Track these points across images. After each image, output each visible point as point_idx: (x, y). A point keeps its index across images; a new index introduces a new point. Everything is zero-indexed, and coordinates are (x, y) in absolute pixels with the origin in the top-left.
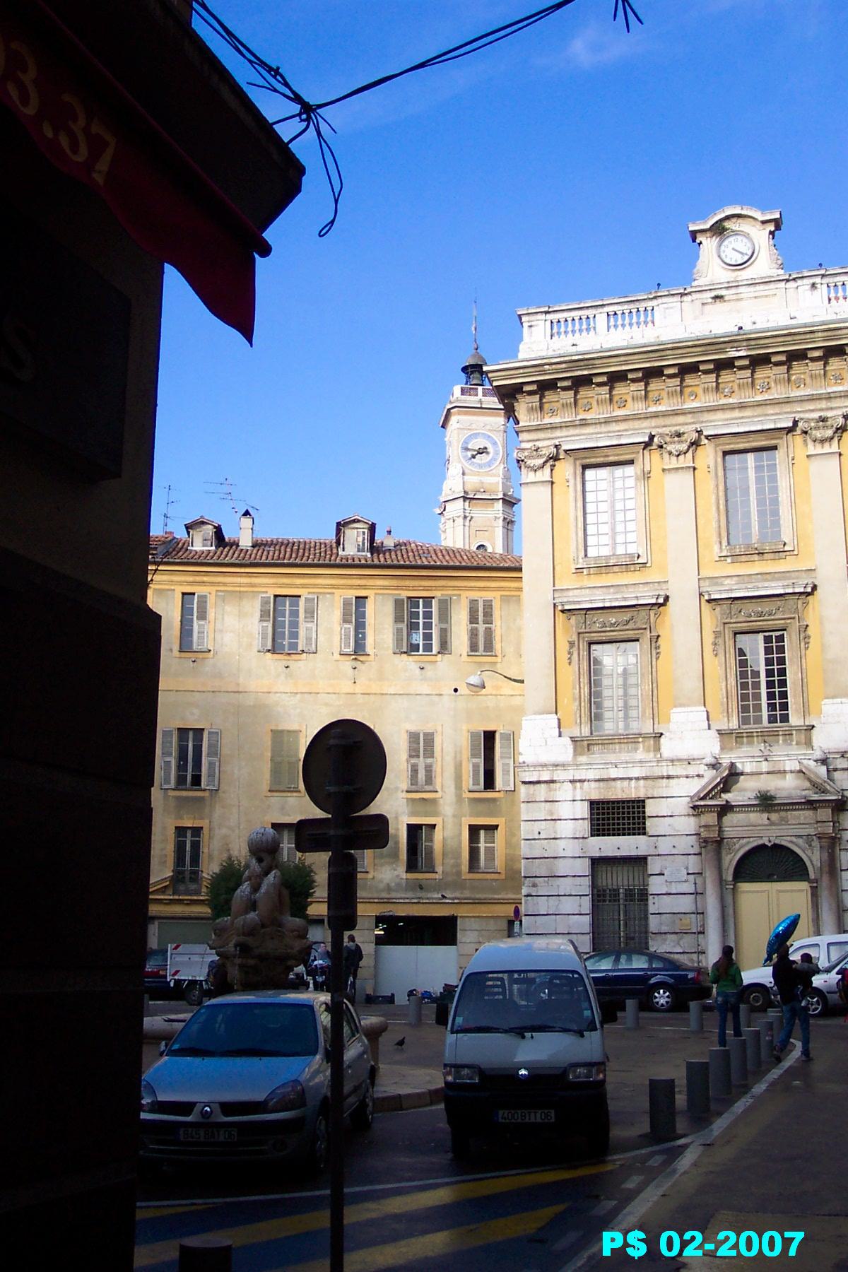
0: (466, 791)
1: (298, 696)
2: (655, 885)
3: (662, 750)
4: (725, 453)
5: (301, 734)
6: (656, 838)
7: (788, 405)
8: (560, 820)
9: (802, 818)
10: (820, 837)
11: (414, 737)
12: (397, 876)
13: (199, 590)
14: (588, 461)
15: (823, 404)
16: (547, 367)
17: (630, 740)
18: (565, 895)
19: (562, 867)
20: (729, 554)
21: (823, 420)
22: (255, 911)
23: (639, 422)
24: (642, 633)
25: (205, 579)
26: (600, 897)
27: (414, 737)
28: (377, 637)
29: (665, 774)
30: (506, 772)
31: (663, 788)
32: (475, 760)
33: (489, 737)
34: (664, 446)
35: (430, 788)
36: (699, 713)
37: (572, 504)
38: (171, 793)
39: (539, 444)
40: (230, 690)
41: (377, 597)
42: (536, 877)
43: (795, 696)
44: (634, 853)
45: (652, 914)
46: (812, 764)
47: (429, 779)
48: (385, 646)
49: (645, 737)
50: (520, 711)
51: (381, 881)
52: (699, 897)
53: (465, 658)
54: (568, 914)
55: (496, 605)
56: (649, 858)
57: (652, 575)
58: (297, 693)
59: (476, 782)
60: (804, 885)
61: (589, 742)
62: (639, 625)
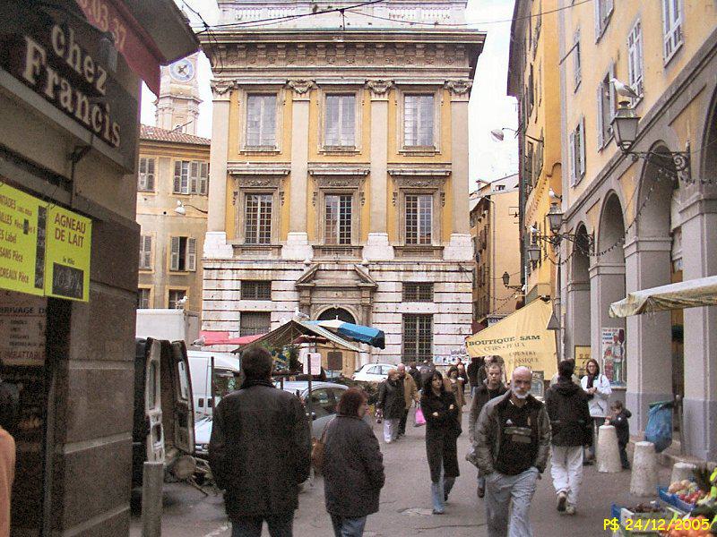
4: (327, 95)
14: (251, 92)
15: (382, 74)
19: (224, 316)
21: (302, 82)
30: (191, 260)
31: (281, 275)
33: (183, 240)
43: (354, 230)
44: (264, 310)
50: (205, 228)
53: (171, 195)
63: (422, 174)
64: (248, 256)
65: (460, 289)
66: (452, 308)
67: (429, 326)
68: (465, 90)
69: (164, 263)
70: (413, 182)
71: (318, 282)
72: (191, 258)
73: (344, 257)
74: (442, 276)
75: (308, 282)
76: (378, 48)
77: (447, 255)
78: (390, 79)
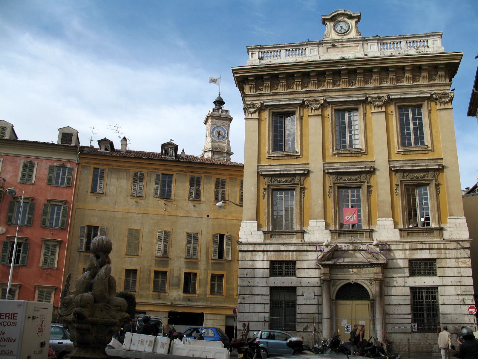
0: (210, 259)
1: (141, 215)
2: (300, 300)
3: (305, 239)
5: (141, 231)
6: (301, 278)
7: (364, 91)
8: (257, 269)
9: (368, 271)
10: (376, 280)
11: (189, 235)
12: (179, 295)
13: (101, 167)
15: (379, 91)
16: (259, 69)
17: (292, 233)
18: (257, 304)
19: (257, 291)
20: (337, 153)
22: (91, 291)
23: (298, 95)
24: (297, 186)
25: (104, 162)
26: (274, 305)
27: (189, 235)
28: (176, 192)
29: (306, 249)
31: (304, 256)
32: (215, 246)
33: (222, 236)
34: (309, 105)
35: (194, 257)
36: (321, 223)
37: (267, 128)
38: (82, 254)
39: (255, 102)
40: (111, 210)
41: (177, 175)
42: (244, 295)
44: (290, 285)
45: (298, 313)
46: (372, 247)
47: (195, 253)
48: (179, 195)
49: (297, 232)
51: (172, 297)
52: (320, 306)
54: (259, 313)
55: (227, 181)
56: (297, 288)
57: (302, 161)
58: (140, 213)
59: (215, 256)
60: (368, 302)
61: (272, 234)
62: (296, 182)
63: (419, 168)
64: (275, 240)
65: (460, 264)
66: (455, 281)
67: (434, 298)
68: (448, 100)
69: (207, 253)
70: (411, 175)
71: (340, 261)
72: (228, 249)
73: (358, 239)
74: (443, 254)
75: (328, 260)
76: (374, 72)
77: (446, 235)
78: (386, 95)
